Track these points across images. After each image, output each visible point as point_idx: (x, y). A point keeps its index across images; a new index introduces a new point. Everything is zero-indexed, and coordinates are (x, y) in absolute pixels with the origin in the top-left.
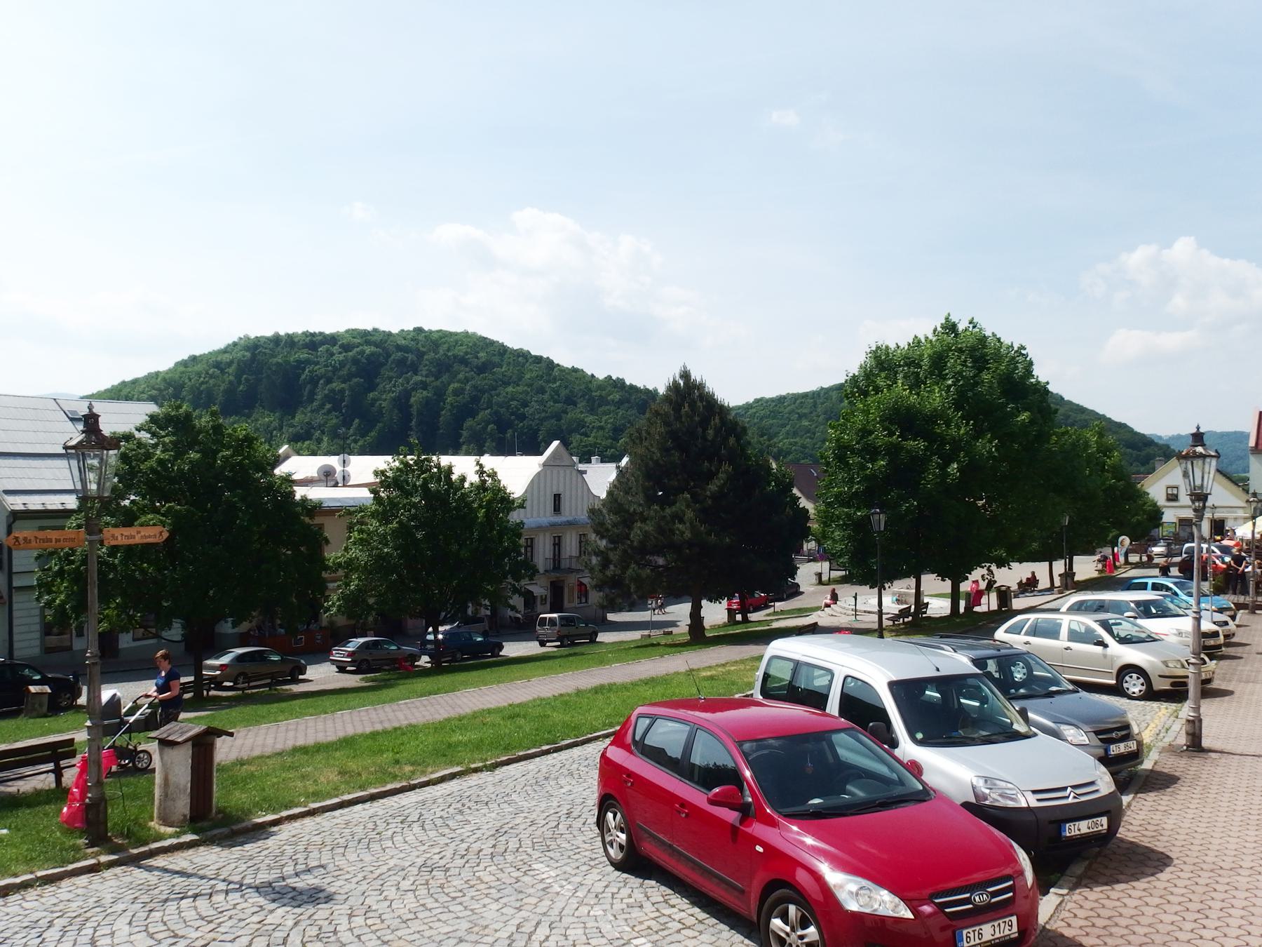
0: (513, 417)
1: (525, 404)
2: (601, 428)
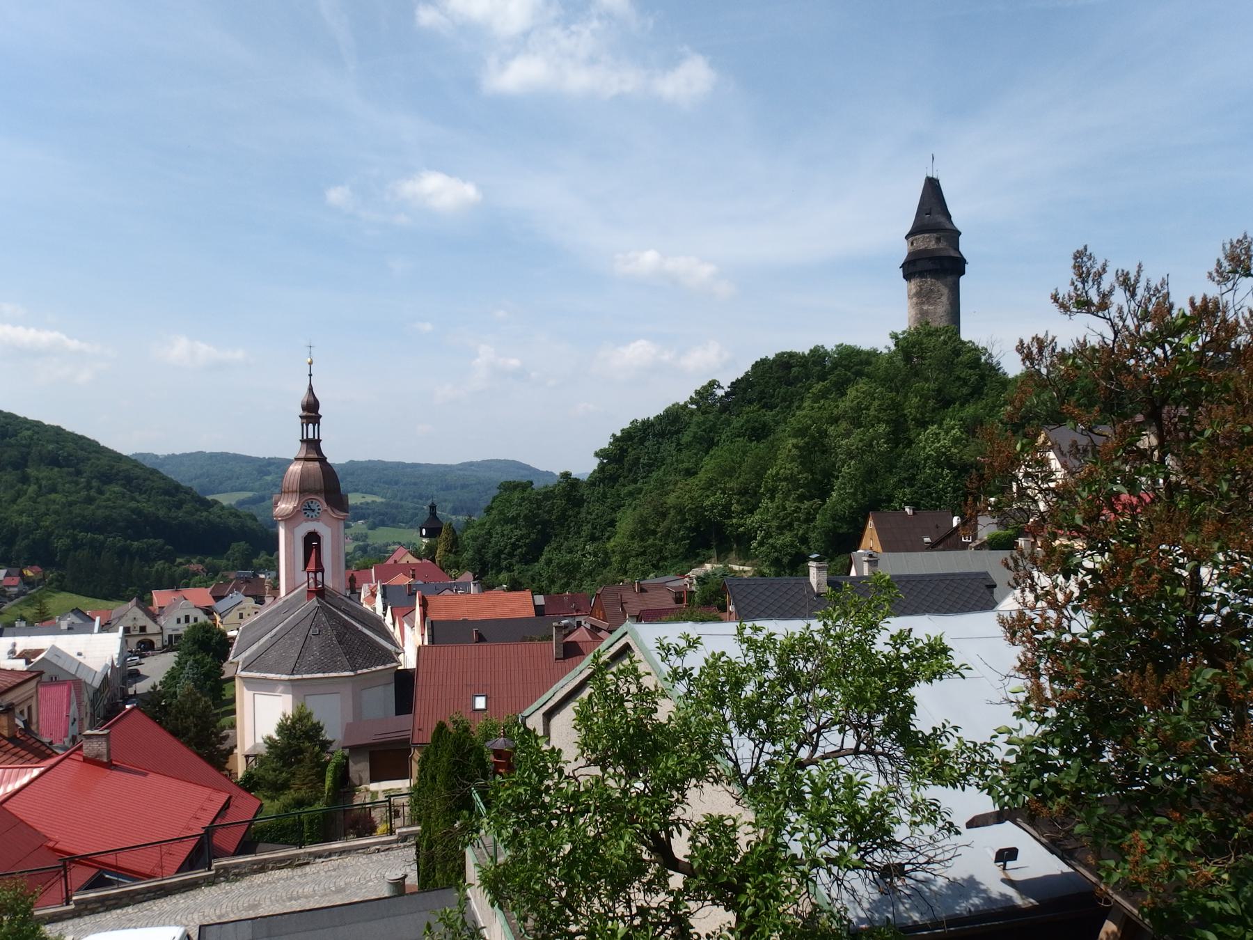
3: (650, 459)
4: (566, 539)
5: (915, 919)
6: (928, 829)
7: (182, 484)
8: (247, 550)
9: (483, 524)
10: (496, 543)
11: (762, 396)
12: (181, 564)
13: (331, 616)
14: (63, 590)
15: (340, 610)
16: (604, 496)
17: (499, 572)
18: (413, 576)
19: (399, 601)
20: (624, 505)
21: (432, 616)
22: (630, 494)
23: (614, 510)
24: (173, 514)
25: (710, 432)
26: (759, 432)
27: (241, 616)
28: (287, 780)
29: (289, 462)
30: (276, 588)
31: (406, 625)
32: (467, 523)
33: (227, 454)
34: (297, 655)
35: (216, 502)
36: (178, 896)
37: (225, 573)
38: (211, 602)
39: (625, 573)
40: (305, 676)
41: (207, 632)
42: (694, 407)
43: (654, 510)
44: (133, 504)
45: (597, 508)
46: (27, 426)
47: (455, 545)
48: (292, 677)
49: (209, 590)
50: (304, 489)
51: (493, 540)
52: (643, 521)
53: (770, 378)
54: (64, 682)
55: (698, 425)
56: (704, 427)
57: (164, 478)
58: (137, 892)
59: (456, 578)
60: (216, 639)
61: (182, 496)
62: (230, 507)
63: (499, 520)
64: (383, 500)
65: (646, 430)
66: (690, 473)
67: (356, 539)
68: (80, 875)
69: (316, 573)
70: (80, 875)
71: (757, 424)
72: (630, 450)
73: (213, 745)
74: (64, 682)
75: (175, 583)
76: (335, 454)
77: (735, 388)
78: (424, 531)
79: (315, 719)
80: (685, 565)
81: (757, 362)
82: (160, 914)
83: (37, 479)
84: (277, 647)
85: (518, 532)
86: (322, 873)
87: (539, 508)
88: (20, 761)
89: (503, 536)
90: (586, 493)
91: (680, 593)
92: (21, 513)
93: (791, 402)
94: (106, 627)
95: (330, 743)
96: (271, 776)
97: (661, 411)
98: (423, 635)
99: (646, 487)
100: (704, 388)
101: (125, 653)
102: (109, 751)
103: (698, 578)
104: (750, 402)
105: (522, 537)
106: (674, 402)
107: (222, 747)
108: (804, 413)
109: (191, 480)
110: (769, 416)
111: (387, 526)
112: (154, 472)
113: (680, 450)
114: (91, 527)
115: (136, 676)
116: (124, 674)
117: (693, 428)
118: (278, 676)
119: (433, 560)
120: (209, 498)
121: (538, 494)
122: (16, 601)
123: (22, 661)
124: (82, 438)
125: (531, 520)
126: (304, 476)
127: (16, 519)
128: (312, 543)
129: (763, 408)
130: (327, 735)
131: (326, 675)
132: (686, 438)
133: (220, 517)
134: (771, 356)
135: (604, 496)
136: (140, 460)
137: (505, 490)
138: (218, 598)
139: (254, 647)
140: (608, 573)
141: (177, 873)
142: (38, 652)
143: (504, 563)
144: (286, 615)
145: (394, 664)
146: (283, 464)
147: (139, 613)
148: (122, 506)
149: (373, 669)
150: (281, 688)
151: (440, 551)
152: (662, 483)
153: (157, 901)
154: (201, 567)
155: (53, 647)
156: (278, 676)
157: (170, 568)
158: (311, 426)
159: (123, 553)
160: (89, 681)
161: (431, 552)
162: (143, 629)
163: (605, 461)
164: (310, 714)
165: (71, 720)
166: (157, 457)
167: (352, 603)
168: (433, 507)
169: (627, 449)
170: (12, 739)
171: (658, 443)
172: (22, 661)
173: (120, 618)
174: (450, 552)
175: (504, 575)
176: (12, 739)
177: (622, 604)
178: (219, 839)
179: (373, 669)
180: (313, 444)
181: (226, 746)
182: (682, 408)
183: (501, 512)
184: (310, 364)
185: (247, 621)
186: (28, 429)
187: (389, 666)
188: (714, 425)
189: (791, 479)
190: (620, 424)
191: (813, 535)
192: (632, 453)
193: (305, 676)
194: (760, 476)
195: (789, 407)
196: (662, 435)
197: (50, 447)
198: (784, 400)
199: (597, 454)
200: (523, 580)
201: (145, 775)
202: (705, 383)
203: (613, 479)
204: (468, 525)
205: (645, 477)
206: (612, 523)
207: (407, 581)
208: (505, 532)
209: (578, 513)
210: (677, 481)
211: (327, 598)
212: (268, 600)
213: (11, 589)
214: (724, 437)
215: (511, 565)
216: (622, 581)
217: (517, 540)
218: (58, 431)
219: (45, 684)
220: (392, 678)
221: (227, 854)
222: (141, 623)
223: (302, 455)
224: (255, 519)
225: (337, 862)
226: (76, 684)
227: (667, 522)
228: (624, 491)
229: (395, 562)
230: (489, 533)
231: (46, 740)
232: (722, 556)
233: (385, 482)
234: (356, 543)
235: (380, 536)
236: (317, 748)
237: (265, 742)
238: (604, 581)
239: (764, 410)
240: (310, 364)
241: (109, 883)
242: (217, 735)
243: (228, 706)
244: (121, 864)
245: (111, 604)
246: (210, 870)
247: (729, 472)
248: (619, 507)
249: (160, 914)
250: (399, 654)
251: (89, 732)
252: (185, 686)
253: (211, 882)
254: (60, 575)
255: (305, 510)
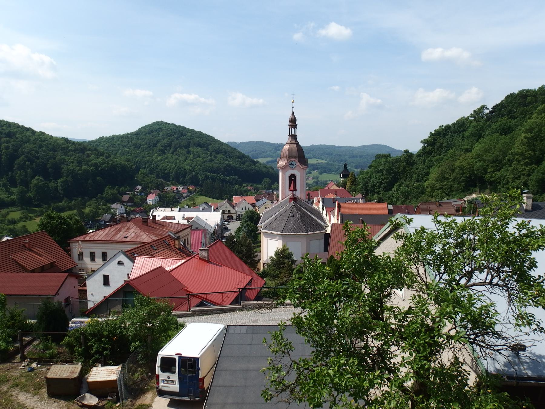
0: (34, 158)
1: (38, 152)
2: (73, 162)
3: (448, 144)
4: (405, 181)
5: (530, 375)
6: (526, 329)
7: (246, 154)
8: (270, 181)
9: (368, 173)
10: (373, 181)
11: (510, 112)
12: (244, 186)
13: (299, 209)
14: (202, 195)
15: (303, 207)
16: (425, 161)
17: (374, 194)
18: (336, 195)
19: (329, 205)
20: (434, 166)
21: (342, 212)
22: (437, 160)
23: (429, 168)
24: (242, 166)
25: (480, 131)
26: (506, 131)
27: (266, 208)
28: (278, 274)
29: (284, 145)
30: (278, 197)
31: (331, 215)
32: (361, 172)
33: (263, 142)
34: (284, 225)
35: (258, 162)
36: (228, 313)
37: (261, 191)
38: (254, 202)
39: (432, 197)
40: (287, 233)
41: (252, 214)
42: (473, 119)
43: (448, 168)
44: (227, 162)
45: (421, 167)
46: (189, 131)
47: (355, 182)
48: (282, 233)
49: (254, 197)
50: (290, 156)
51: (371, 180)
52: (443, 173)
53: (515, 103)
54: (200, 230)
55: (474, 127)
56: (477, 129)
57: (238, 152)
58: (214, 310)
59: (354, 196)
60: (256, 216)
61: (245, 159)
62: (264, 164)
63: (375, 171)
64: (326, 162)
65: (447, 130)
66: (468, 151)
67: (314, 178)
68: (197, 301)
69: (293, 191)
70: (197, 301)
71: (505, 127)
72: (438, 139)
73: (252, 258)
74: (200, 230)
75: (242, 194)
76: (303, 141)
77: (495, 109)
78: (341, 175)
79: (290, 251)
80: (462, 194)
81: (508, 95)
82: (221, 319)
83: (193, 152)
84: (276, 221)
85: (383, 177)
86: (283, 312)
87: (393, 166)
88: (182, 257)
89: (376, 178)
90: (416, 159)
91: (459, 207)
92: (188, 165)
93: (526, 115)
94: (216, 210)
95: (296, 261)
96: (272, 272)
97: (454, 121)
98: (338, 220)
99: (445, 157)
100: (478, 109)
101: (223, 220)
102: (208, 256)
103: (468, 201)
104: (503, 116)
105: (385, 178)
106: (462, 117)
107: (256, 259)
108: (532, 120)
109: (249, 153)
110: (513, 122)
111: (327, 173)
112: (235, 149)
113: (464, 140)
114: (212, 171)
115: (226, 229)
116: (222, 228)
117: (471, 129)
118: (277, 233)
119: (345, 188)
120: (256, 160)
121: (393, 160)
122: (186, 198)
123: (187, 221)
124: (209, 136)
125: (389, 171)
126: (290, 151)
127: (186, 168)
128: (293, 178)
129: (510, 118)
130: (295, 258)
131: (296, 233)
132: (467, 134)
133: (259, 168)
134: (516, 92)
135: (425, 161)
136: (230, 145)
137: (378, 158)
138: (257, 200)
139: (268, 220)
140: (424, 197)
141: (230, 304)
142: (192, 218)
143: (376, 190)
144: (281, 208)
145: (324, 231)
146: (282, 146)
147: (228, 205)
148: (223, 163)
149: (315, 232)
150: (278, 238)
151: (348, 184)
152: (453, 156)
153: (221, 314)
154: (252, 188)
155: (197, 216)
156: (277, 233)
157: (240, 188)
158: (293, 129)
159: (223, 181)
160: (209, 230)
161: (344, 185)
162: (229, 211)
163: (426, 145)
164: (288, 249)
165: (202, 244)
166: (236, 143)
167: (308, 204)
168: (346, 165)
169: (437, 139)
170: (179, 249)
171: (453, 136)
172: (187, 221)
173: (221, 207)
174: (352, 185)
175: (376, 196)
176: (179, 249)
177: (429, 211)
178: (248, 294)
179: (315, 232)
180: (294, 137)
181: (257, 259)
182: (466, 119)
183: (376, 168)
184: (293, 102)
185: (268, 209)
186: (189, 133)
187: (321, 231)
188: (483, 127)
189: (521, 154)
190: (434, 127)
191: (530, 183)
192: (439, 141)
193: (287, 233)
194: (505, 154)
195: (524, 117)
196: (455, 132)
197: (197, 139)
198: (521, 114)
199: (422, 142)
200: (384, 198)
201: (221, 266)
202: (479, 107)
203: (429, 153)
204: (361, 173)
205: (445, 153)
206: (428, 174)
207: (333, 196)
208: (377, 177)
209: (412, 169)
210: (461, 155)
211: (298, 202)
212: (275, 202)
213: (184, 194)
214: (487, 133)
215: (379, 191)
216: (430, 200)
217: (382, 180)
218: (200, 133)
219: (194, 230)
220: (323, 237)
221: (250, 300)
222: (228, 209)
223: (289, 142)
224: (273, 169)
225: (289, 309)
226: (205, 231)
227: (454, 175)
228: (434, 159)
229: (329, 188)
230: (370, 177)
231: (191, 251)
232: (482, 190)
233: (327, 154)
234: (314, 180)
235: (324, 177)
236: (290, 263)
237: (270, 258)
238: (422, 200)
239: (510, 120)
240: (293, 102)
241: (206, 305)
242: (253, 254)
243: (257, 242)
244: (208, 298)
245: (219, 201)
246: (240, 305)
247: (488, 151)
248: (431, 166)
249: (221, 319)
250: (326, 227)
251: (201, 248)
252: (242, 234)
253: (241, 310)
254: (201, 189)
255: (290, 165)
